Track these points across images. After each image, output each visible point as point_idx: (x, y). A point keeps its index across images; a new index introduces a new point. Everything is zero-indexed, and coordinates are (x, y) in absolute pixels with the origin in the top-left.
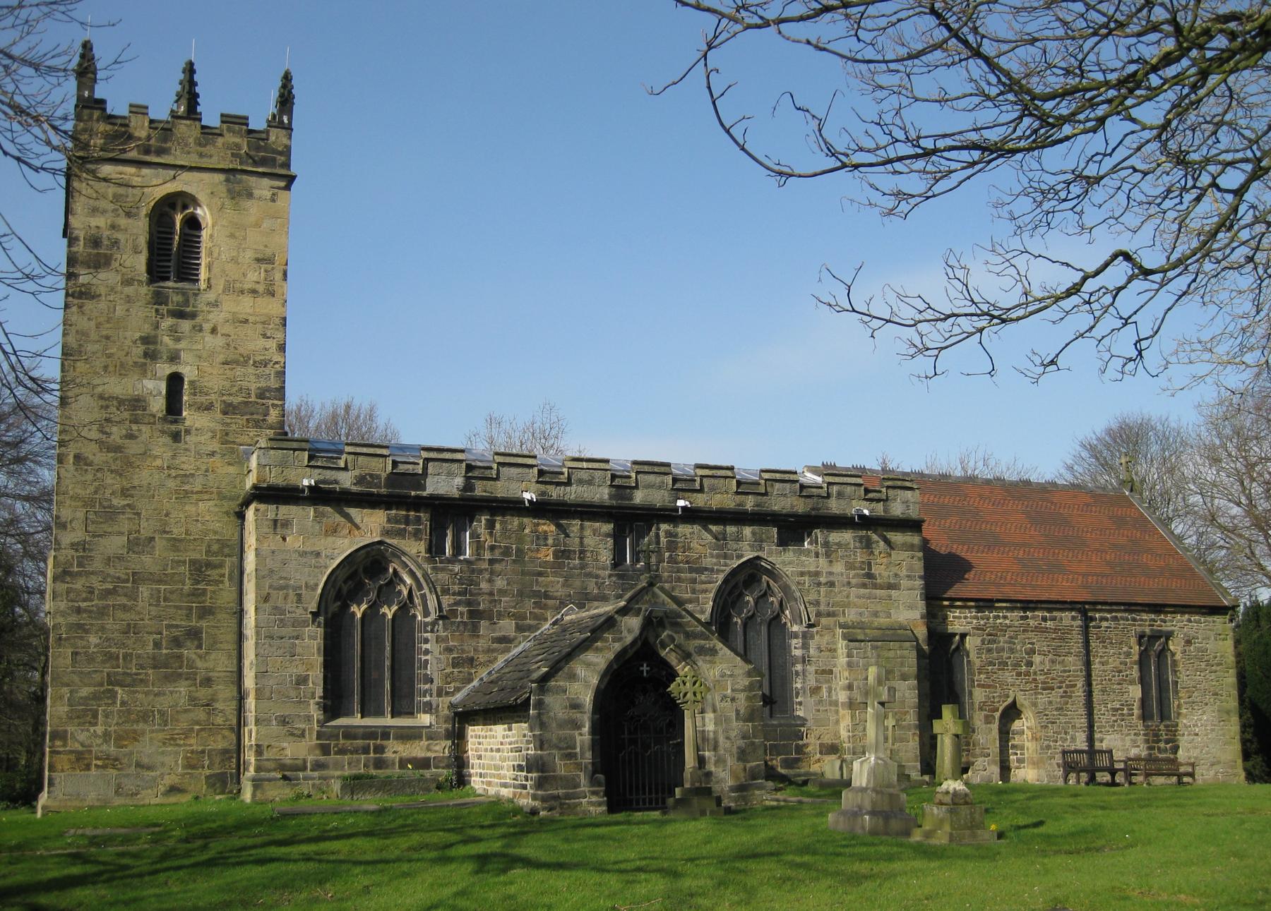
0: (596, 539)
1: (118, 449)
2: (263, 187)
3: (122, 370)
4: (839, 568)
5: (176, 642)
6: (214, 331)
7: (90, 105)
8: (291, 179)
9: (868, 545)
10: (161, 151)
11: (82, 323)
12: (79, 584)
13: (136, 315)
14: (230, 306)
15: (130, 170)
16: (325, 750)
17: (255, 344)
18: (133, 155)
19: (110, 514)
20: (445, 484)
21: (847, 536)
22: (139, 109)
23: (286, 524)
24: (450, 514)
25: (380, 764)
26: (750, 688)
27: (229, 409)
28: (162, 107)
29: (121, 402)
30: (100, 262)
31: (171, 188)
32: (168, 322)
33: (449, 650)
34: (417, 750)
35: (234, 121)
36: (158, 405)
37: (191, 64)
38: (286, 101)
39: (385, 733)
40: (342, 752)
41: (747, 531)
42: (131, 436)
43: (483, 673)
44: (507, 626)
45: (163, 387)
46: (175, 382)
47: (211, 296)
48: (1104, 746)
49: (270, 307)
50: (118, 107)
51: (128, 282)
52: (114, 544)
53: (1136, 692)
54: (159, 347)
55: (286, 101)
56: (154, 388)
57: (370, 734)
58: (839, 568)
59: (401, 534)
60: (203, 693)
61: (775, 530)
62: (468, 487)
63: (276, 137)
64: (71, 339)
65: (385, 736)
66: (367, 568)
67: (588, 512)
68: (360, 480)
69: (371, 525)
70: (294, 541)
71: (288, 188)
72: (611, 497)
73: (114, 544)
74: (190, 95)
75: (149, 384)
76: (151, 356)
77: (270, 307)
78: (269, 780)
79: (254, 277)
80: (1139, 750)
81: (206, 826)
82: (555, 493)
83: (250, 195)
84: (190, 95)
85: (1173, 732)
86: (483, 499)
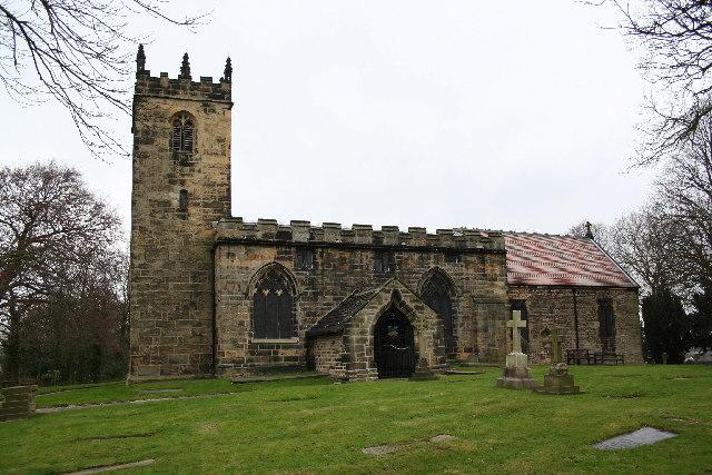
0: (367, 258)
1: (159, 223)
2: (218, 108)
3: (161, 188)
4: (471, 271)
5: (185, 307)
6: (199, 171)
7: (142, 73)
8: (232, 104)
9: (483, 262)
10: (175, 93)
11: (143, 169)
12: (142, 283)
13: (167, 166)
14: (205, 160)
15: (162, 101)
16: (252, 353)
17: (218, 178)
18: (163, 95)
19: (156, 252)
20: (301, 237)
21: (474, 258)
22: (164, 75)
23: (233, 255)
24: (302, 248)
25: (276, 359)
26: (439, 323)
27: (206, 205)
28: (174, 74)
29: (159, 203)
30: (149, 142)
31: (179, 109)
32: (179, 168)
33: (305, 309)
34: (291, 353)
35: (207, 80)
36: (176, 203)
37: (186, 55)
38: (228, 71)
39: (278, 346)
40: (260, 354)
41: (432, 255)
42: (164, 217)
43: (319, 319)
44: (329, 298)
45: (178, 196)
46: (184, 192)
47: (197, 156)
48: (585, 347)
49: (223, 161)
50: (155, 74)
51: (161, 150)
52: (158, 264)
53: (597, 325)
54: (517, 267)
55: (228, 71)
56: (174, 197)
57: (271, 346)
58: (471, 271)
59: (282, 259)
60: (198, 330)
61: (687, 313)
62: (312, 237)
63: (224, 87)
64: (137, 176)
65: (278, 347)
66: (272, 276)
67: (363, 248)
68: (265, 235)
69: (269, 255)
70: (237, 262)
71: (230, 109)
72: (374, 241)
73: (158, 264)
74: (185, 68)
75: (172, 194)
76: (172, 182)
77: (223, 161)
78: (228, 367)
79: (218, 147)
80: (600, 350)
81: (271, 378)
82: (349, 240)
83: (214, 111)
84: (185, 68)
85: (613, 341)
86: (319, 243)
